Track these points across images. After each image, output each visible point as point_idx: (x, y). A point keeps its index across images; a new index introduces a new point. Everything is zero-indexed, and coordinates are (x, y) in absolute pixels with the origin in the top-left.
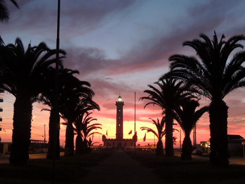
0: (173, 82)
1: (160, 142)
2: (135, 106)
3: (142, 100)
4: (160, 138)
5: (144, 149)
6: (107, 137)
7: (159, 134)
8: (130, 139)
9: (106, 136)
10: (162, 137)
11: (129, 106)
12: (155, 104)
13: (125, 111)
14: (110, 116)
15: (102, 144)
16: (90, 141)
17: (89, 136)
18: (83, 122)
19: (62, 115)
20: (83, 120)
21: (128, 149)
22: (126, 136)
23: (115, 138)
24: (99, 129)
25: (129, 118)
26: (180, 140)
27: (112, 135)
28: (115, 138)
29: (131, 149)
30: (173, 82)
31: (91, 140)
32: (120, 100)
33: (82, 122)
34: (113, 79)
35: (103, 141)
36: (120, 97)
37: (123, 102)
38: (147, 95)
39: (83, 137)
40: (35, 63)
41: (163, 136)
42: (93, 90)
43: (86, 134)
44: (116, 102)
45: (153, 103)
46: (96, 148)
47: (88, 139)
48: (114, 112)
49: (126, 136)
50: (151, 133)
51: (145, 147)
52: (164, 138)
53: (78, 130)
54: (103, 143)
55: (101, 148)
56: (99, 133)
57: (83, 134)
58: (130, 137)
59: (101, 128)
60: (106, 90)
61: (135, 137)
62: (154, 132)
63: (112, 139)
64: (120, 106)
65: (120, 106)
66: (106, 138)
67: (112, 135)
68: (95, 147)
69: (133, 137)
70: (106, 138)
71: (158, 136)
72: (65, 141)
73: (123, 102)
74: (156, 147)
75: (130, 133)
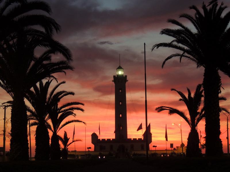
0: (217, 10)
1: (193, 136)
2: (146, 88)
3: (158, 48)
4: (193, 125)
5: (163, 154)
6: (101, 138)
7: (191, 117)
8: (140, 139)
9: (98, 134)
10: (197, 123)
11: (136, 88)
12: (183, 58)
13: (130, 96)
14: (107, 105)
15: (90, 148)
16: (66, 140)
17: (61, 128)
18: (49, 99)
19: (4, 82)
20: (48, 96)
21: (134, 155)
22: (134, 133)
23: (114, 137)
24: (56, 81)
25: (136, 107)
26: (227, 136)
27: (108, 133)
28: (114, 137)
29: (140, 155)
30: (217, 10)
31: (66, 135)
32: (120, 73)
33: (47, 100)
34: (111, 44)
35: (92, 143)
36: (120, 68)
37: (126, 76)
38: (169, 39)
39: (51, 129)
40: (29, 67)
41: (199, 120)
42: (58, 21)
43: (57, 123)
44: (114, 77)
45: (178, 55)
46: (81, 156)
47: (60, 133)
48: (112, 98)
49: (134, 133)
50: (176, 116)
51: (165, 152)
52: (201, 126)
53: (39, 116)
54: (93, 146)
55: (89, 155)
56: (81, 122)
57: (50, 122)
58: (139, 135)
59: (82, 110)
60: (100, 62)
61: (148, 135)
62: (182, 114)
63: (109, 140)
64: (120, 85)
65: (120, 85)
66: (99, 138)
67: (108, 133)
68: (80, 154)
69: (144, 135)
70: (99, 138)
71: (190, 122)
72: (10, 133)
73: (126, 76)
74: (185, 151)
75: (140, 128)
